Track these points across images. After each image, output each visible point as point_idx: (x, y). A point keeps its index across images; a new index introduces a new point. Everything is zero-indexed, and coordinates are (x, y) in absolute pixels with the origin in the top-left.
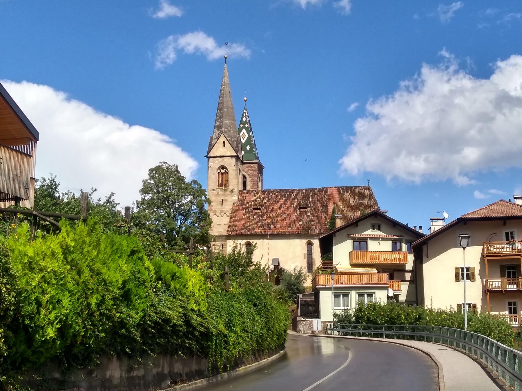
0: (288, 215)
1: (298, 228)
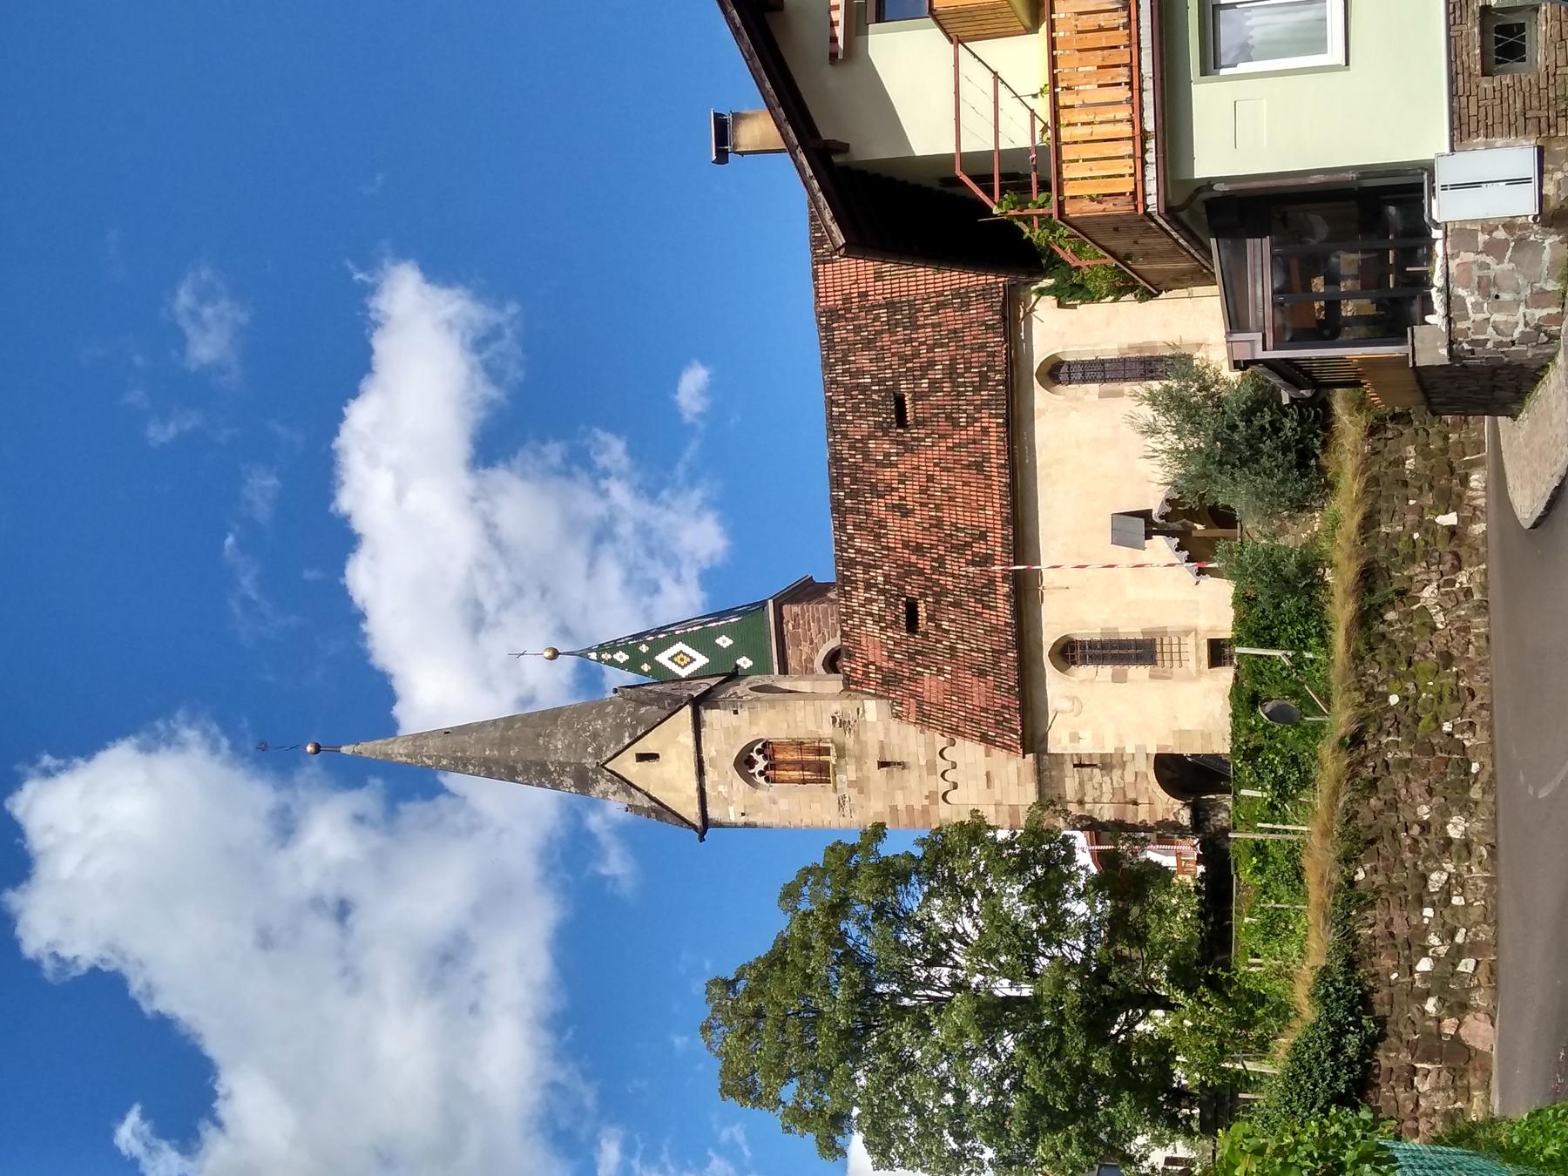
0: (930, 479)
1: (985, 431)
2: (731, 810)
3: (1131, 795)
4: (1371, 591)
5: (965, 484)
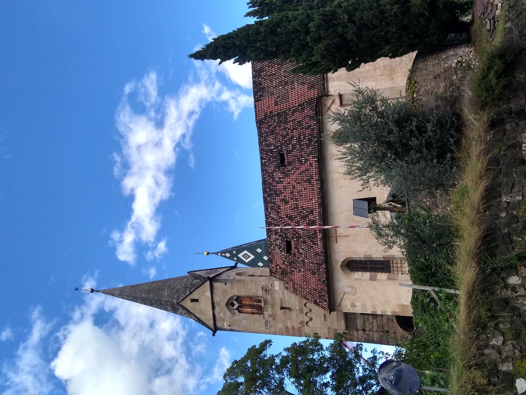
0: (294, 187)
1: (311, 165)
2: (225, 323)
3: (386, 328)
4: (493, 255)
5: (305, 189)
